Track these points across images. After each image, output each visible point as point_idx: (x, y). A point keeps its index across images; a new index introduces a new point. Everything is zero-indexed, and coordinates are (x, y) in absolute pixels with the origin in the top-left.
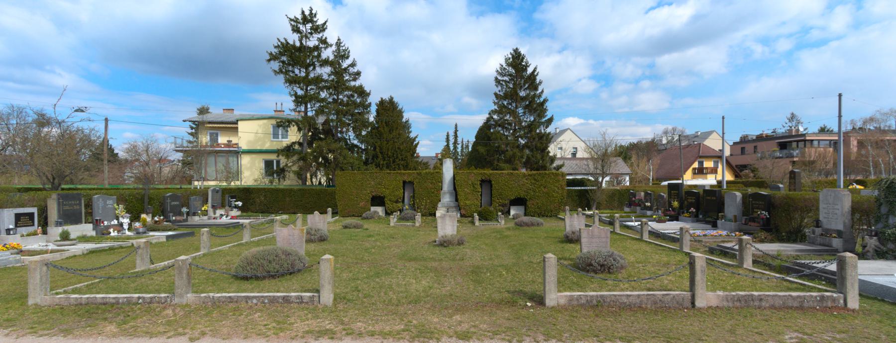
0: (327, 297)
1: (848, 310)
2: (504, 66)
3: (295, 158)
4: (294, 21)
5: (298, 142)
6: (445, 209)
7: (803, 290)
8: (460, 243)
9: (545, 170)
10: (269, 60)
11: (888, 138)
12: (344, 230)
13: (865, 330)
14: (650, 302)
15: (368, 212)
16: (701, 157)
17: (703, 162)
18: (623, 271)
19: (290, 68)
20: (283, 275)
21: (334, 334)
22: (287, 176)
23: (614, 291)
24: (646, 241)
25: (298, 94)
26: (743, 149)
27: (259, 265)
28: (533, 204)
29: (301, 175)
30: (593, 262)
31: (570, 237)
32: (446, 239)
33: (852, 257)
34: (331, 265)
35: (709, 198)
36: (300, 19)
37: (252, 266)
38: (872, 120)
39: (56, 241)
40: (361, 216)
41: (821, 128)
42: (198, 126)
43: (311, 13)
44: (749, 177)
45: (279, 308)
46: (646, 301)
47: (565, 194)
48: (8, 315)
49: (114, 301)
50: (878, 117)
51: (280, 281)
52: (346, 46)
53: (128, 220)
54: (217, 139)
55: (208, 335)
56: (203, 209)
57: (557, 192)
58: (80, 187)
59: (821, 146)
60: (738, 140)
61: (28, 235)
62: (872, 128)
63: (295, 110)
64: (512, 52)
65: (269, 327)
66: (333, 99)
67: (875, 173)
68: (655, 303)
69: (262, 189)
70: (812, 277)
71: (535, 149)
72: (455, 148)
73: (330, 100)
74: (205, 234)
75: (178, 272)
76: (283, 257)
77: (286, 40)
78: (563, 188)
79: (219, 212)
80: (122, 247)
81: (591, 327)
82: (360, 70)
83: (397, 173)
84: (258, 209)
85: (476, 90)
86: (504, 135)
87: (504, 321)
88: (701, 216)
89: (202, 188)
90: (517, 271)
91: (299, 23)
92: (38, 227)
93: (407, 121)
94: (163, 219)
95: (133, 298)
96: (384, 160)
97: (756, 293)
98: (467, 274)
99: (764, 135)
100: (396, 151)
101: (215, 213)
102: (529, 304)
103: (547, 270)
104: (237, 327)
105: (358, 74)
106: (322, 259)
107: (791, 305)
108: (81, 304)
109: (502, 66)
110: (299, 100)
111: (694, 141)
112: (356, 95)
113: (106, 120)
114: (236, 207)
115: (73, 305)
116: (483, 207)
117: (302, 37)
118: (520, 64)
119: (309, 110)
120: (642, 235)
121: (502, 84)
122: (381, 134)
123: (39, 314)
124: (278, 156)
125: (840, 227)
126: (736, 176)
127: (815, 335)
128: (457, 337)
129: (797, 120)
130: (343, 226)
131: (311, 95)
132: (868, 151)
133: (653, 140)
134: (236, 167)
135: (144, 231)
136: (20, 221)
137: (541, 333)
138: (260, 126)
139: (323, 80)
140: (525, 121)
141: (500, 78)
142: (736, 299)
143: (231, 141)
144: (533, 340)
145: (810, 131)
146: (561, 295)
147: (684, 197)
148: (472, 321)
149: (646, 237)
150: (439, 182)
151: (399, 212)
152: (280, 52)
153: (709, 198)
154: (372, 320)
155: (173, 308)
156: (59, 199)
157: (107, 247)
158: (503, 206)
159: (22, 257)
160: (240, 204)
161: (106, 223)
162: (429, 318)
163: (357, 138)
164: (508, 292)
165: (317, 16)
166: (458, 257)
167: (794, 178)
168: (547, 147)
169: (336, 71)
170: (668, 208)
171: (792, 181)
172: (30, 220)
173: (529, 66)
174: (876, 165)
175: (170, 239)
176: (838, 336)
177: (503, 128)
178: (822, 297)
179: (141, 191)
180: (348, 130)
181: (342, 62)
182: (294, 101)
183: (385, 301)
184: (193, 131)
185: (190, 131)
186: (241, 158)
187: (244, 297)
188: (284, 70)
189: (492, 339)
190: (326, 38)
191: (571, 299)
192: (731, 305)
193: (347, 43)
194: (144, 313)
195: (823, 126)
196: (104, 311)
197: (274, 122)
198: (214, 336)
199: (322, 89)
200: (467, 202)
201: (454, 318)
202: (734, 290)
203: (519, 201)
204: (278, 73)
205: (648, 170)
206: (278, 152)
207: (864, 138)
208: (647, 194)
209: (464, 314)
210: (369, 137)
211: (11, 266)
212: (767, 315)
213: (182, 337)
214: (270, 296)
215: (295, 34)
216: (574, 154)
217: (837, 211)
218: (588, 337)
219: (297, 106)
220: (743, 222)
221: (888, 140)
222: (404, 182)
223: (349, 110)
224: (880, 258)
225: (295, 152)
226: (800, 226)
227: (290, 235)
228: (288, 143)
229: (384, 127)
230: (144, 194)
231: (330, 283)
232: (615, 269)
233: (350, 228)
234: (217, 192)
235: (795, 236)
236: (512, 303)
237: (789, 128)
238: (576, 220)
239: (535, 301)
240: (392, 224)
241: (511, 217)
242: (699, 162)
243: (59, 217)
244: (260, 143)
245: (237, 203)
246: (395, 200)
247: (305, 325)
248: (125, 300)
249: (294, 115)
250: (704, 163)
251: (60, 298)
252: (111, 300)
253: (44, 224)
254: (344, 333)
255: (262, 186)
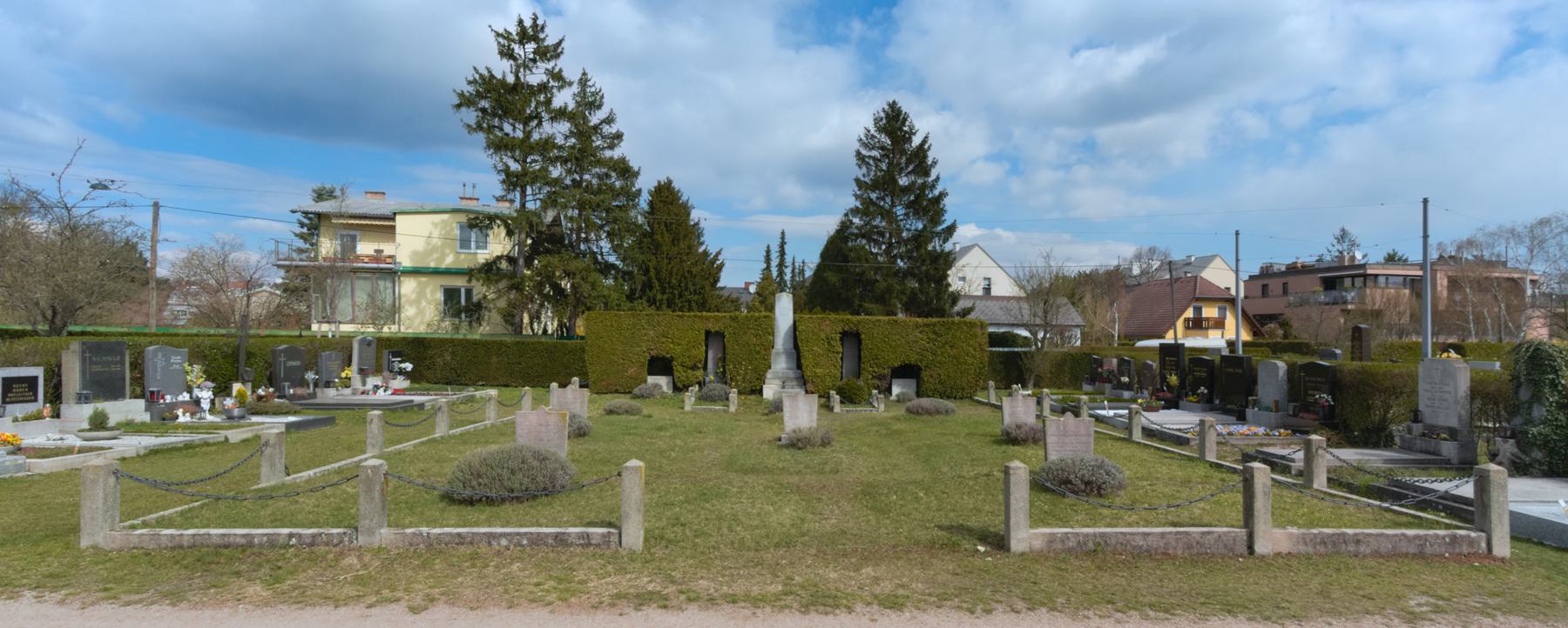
0: (634, 535)
1: (1495, 559)
2: (872, 132)
3: (503, 284)
4: (504, 38)
5: (507, 256)
6: (778, 382)
7: (1420, 526)
8: (825, 443)
9: (943, 316)
10: (459, 106)
11: (1497, 275)
12: (607, 417)
13: (1530, 592)
14: (1180, 545)
15: (643, 386)
16: (1198, 299)
17: (1200, 308)
18: (1122, 493)
19: (496, 122)
20: (535, 497)
21: (666, 599)
22: (486, 318)
23: (1116, 526)
24: (1138, 443)
25: (512, 169)
26: (1265, 287)
27: (494, 479)
28: (932, 377)
29: (513, 316)
30: (1072, 477)
31: (1014, 434)
32: (800, 435)
33: (1499, 471)
34: (641, 478)
35: (1231, 370)
36: (514, 33)
37: (480, 480)
38: (1470, 243)
39: (83, 431)
40: (630, 392)
41: (1389, 255)
42: (314, 224)
43: (535, 25)
44: (1276, 336)
45: (551, 555)
46: (1174, 544)
47: (986, 359)
48: (49, 566)
49: (243, 541)
50: (1481, 239)
51: (531, 507)
52: (598, 86)
53: (210, 393)
54: (355, 247)
55: (441, 602)
56: (343, 375)
57: (973, 356)
58: (89, 329)
59: (1390, 286)
60: (1256, 272)
61: (26, 419)
62: (1470, 257)
63: (500, 199)
64: (886, 107)
65: (546, 587)
66: (574, 181)
67: (1477, 334)
68: (1190, 547)
69: (447, 339)
70: (1423, 505)
71: (925, 280)
72: (781, 273)
73: (568, 182)
74: (375, 420)
75: (365, 488)
76: (536, 463)
77: (490, 72)
78: (982, 349)
79: (372, 381)
80: (207, 444)
81: (1095, 587)
82: (622, 130)
83: (695, 316)
84: (439, 376)
85: (813, 173)
86: (872, 253)
87: (950, 577)
88: (1217, 402)
89: (337, 336)
90: (943, 493)
91: (513, 41)
92: (45, 403)
93: (697, 224)
94: (274, 392)
95: (279, 535)
96: (663, 293)
97: (1350, 531)
98: (856, 496)
99: (1299, 265)
100: (686, 278)
101: (364, 384)
102: (981, 548)
103: (1013, 489)
104: (487, 587)
105: (619, 136)
106: (626, 467)
107: (1405, 550)
108: (181, 547)
109: (869, 131)
110: (514, 181)
111: (1186, 273)
112: (613, 174)
113: (156, 206)
114: (401, 372)
115: (165, 549)
116: (845, 380)
117: (518, 67)
118: (901, 129)
119: (528, 198)
120: (1131, 433)
121: (868, 163)
122: (658, 246)
123: (108, 565)
124: (470, 281)
125: (1453, 422)
126: (1255, 334)
127: (1455, 600)
128: (879, 605)
129: (1350, 241)
130: (605, 410)
131: (534, 172)
132: (1466, 295)
133: (1118, 268)
134: (391, 300)
135: (241, 414)
136: (11, 392)
137: (1017, 596)
138: (435, 225)
139: (555, 146)
140: (907, 229)
141: (864, 152)
142: (1318, 540)
143: (382, 251)
144: (1009, 609)
145: (1372, 260)
146: (1035, 534)
147: (1187, 368)
148: (896, 577)
149: (1137, 435)
150: (769, 334)
151: (697, 386)
152: (477, 91)
153: (1231, 370)
154: (723, 576)
155: (357, 553)
156: (83, 352)
157: (181, 442)
158: (880, 379)
159: (28, 460)
160: (409, 366)
161: (168, 398)
162: (820, 571)
163: (615, 251)
164: (940, 527)
165: (546, 30)
166: (828, 468)
167: (1360, 338)
168: (945, 276)
169: (578, 130)
170: (1159, 387)
171: (1357, 343)
172: (29, 391)
173: (915, 134)
174: (1479, 320)
175: (292, 430)
176: (1490, 601)
177: (870, 240)
178: (1454, 538)
179: (234, 339)
180: (598, 239)
181: (590, 114)
182: (503, 182)
183: (732, 543)
184: (305, 230)
185: (298, 230)
186: (400, 282)
187: (484, 534)
188: (485, 125)
189: (939, 607)
190: (561, 70)
191: (1052, 539)
192: (1310, 550)
193: (598, 81)
194: (307, 563)
195: (1391, 252)
196: (231, 559)
197: (463, 218)
198: (453, 604)
199: (553, 161)
200: (818, 371)
201: (863, 571)
202: (1312, 525)
203: (906, 371)
204: (475, 130)
205: (1112, 320)
206: (469, 273)
207: (1460, 274)
208: (1122, 362)
209: (877, 565)
210: (636, 250)
211: (7, 476)
212: (1372, 568)
213: (393, 606)
214: (531, 533)
215: (505, 60)
216: (987, 290)
217: (1446, 396)
218: (1098, 603)
219: (508, 191)
220: (1291, 413)
221: (1497, 278)
222: (708, 333)
223: (603, 202)
224: (1521, 476)
225: (500, 275)
226: (1384, 420)
227: (541, 425)
228: (488, 257)
229: (662, 234)
230: (238, 346)
231: (639, 511)
232: (1110, 490)
233: (618, 414)
234: (369, 344)
235: (1375, 437)
236: (953, 548)
237: (1337, 254)
238: (1020, 404)
239: (989, 543)
240: (688, 408)
241: (893, 397)
242: (1195, 308)
243: (84, 387)
244: (435, 256)
245: (403, 365)
246: (690, 364)
247: (607, 584)
248: (265, 539)
249: (505, 208)
250: (1203, 309)
251: (143, 535)
252: (238, 540)
253: (55, 396)
254: (683, 597)
255: (441, 334)
